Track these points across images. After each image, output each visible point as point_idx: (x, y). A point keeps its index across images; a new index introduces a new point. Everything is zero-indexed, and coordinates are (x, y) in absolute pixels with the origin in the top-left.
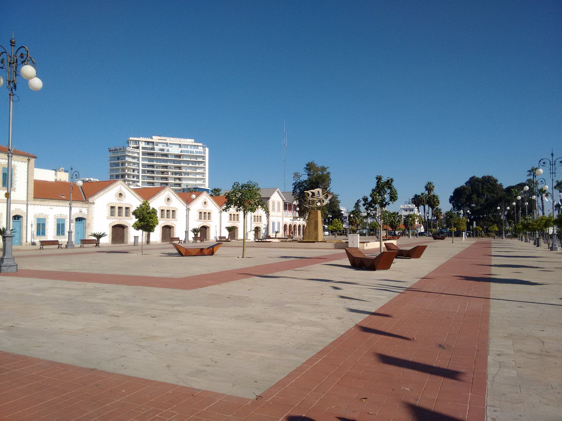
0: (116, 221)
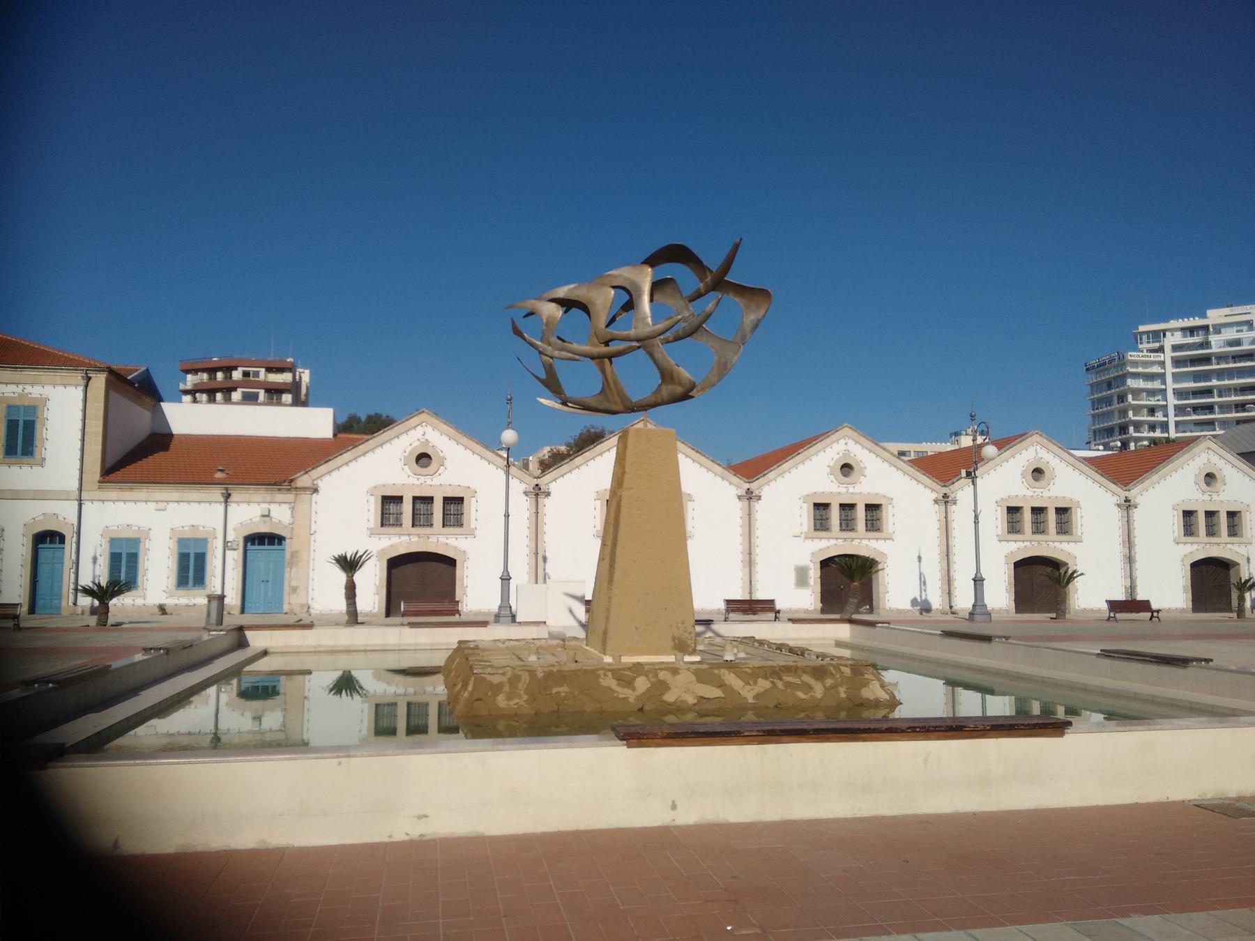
0: (835, 544)
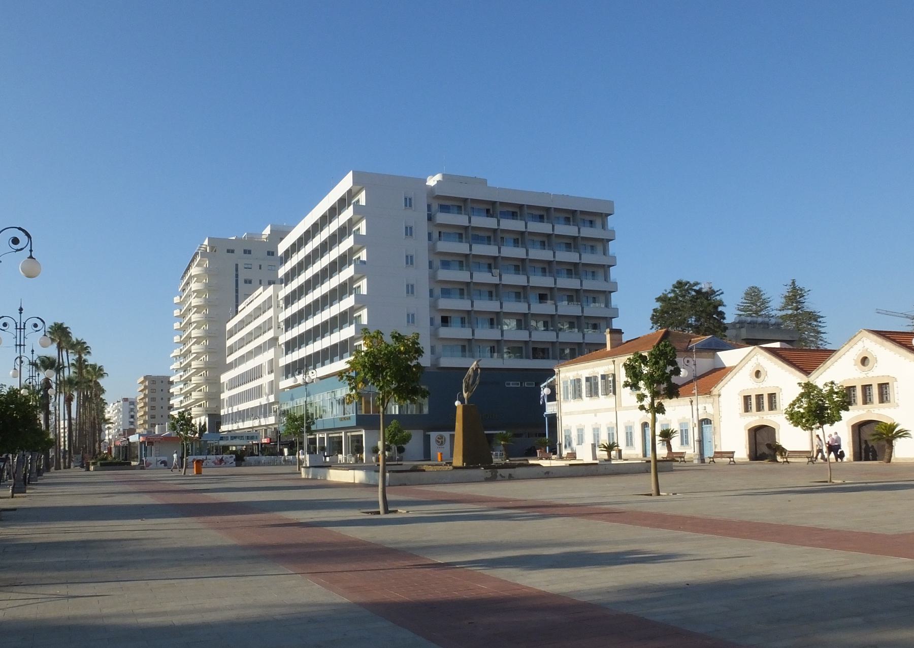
0: (755, 419)
